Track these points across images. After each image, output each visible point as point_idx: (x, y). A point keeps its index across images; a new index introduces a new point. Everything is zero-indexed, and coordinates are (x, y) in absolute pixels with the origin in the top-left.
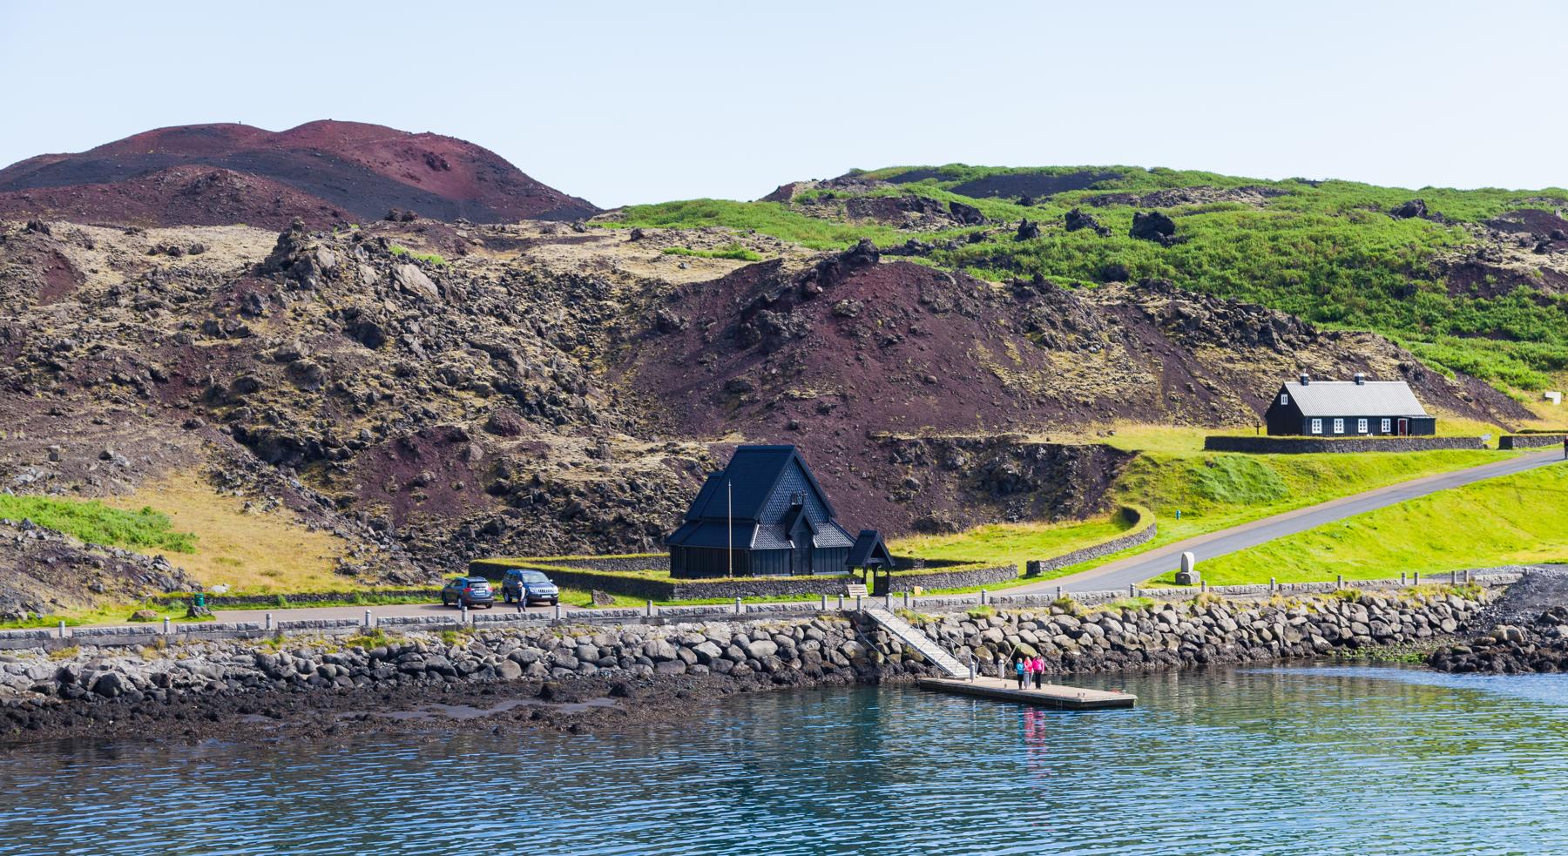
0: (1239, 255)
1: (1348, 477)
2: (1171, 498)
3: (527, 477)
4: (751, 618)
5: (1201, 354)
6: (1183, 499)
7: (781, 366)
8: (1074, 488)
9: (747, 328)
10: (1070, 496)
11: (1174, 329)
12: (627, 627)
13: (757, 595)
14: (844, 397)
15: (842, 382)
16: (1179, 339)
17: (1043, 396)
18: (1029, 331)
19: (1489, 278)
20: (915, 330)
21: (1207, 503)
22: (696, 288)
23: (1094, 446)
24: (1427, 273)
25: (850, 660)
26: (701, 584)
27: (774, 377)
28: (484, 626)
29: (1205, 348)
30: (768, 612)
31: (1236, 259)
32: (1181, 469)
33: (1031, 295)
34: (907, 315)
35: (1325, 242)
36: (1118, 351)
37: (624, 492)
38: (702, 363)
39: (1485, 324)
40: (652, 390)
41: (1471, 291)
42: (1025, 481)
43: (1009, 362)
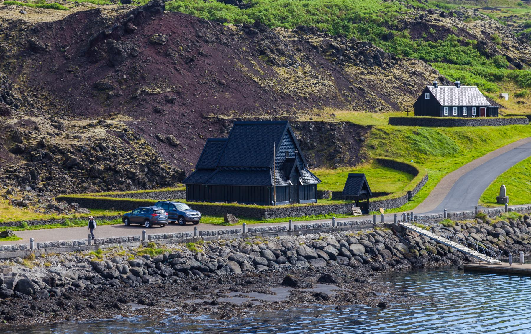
0: (289, 15)
1: (485, 140)
2: (403, 153)
3: (34, 143)
4: (342, 230)
5: (348, 70)
6: (409, 154)
7: (128, 74)
8: (340, 147)
9: (96, 50)
10: (340, 153)
11: (330, 55)
12: (282, 237)
13: (306, 215)
14: (178, 93)
15: (173, 84)
16: (334, 61)
17: (283, 93)
18: (260, 55)
19: (432, 30)
20: (202, 53)
21: (423, 156)
22: (48, 26)
23: (343, 122)
24: (397, 27)
25: (403, 254)
26: (279, 209)
27: (126, 80)
28: (208, 239)
29: (348, 66)
30: (348, 226)
31: (288, 17)
32: (402, 136)
33: (255, 34)
34: (194, 44)
35: (334, 8)
36: (308, 68)
37: (96, 151)
38: (70, 72)
39: (437, 55)
40: (43, 88)
41: (424, 38)
42: (306, 144)
43: (257, 73)
